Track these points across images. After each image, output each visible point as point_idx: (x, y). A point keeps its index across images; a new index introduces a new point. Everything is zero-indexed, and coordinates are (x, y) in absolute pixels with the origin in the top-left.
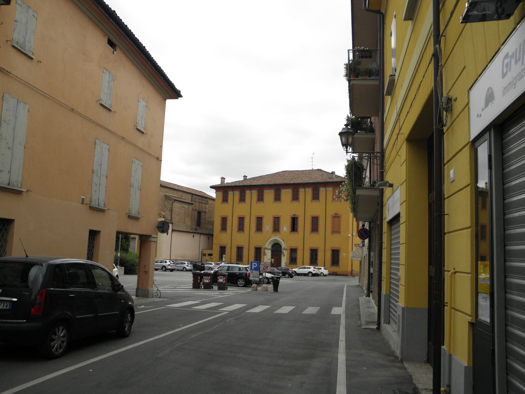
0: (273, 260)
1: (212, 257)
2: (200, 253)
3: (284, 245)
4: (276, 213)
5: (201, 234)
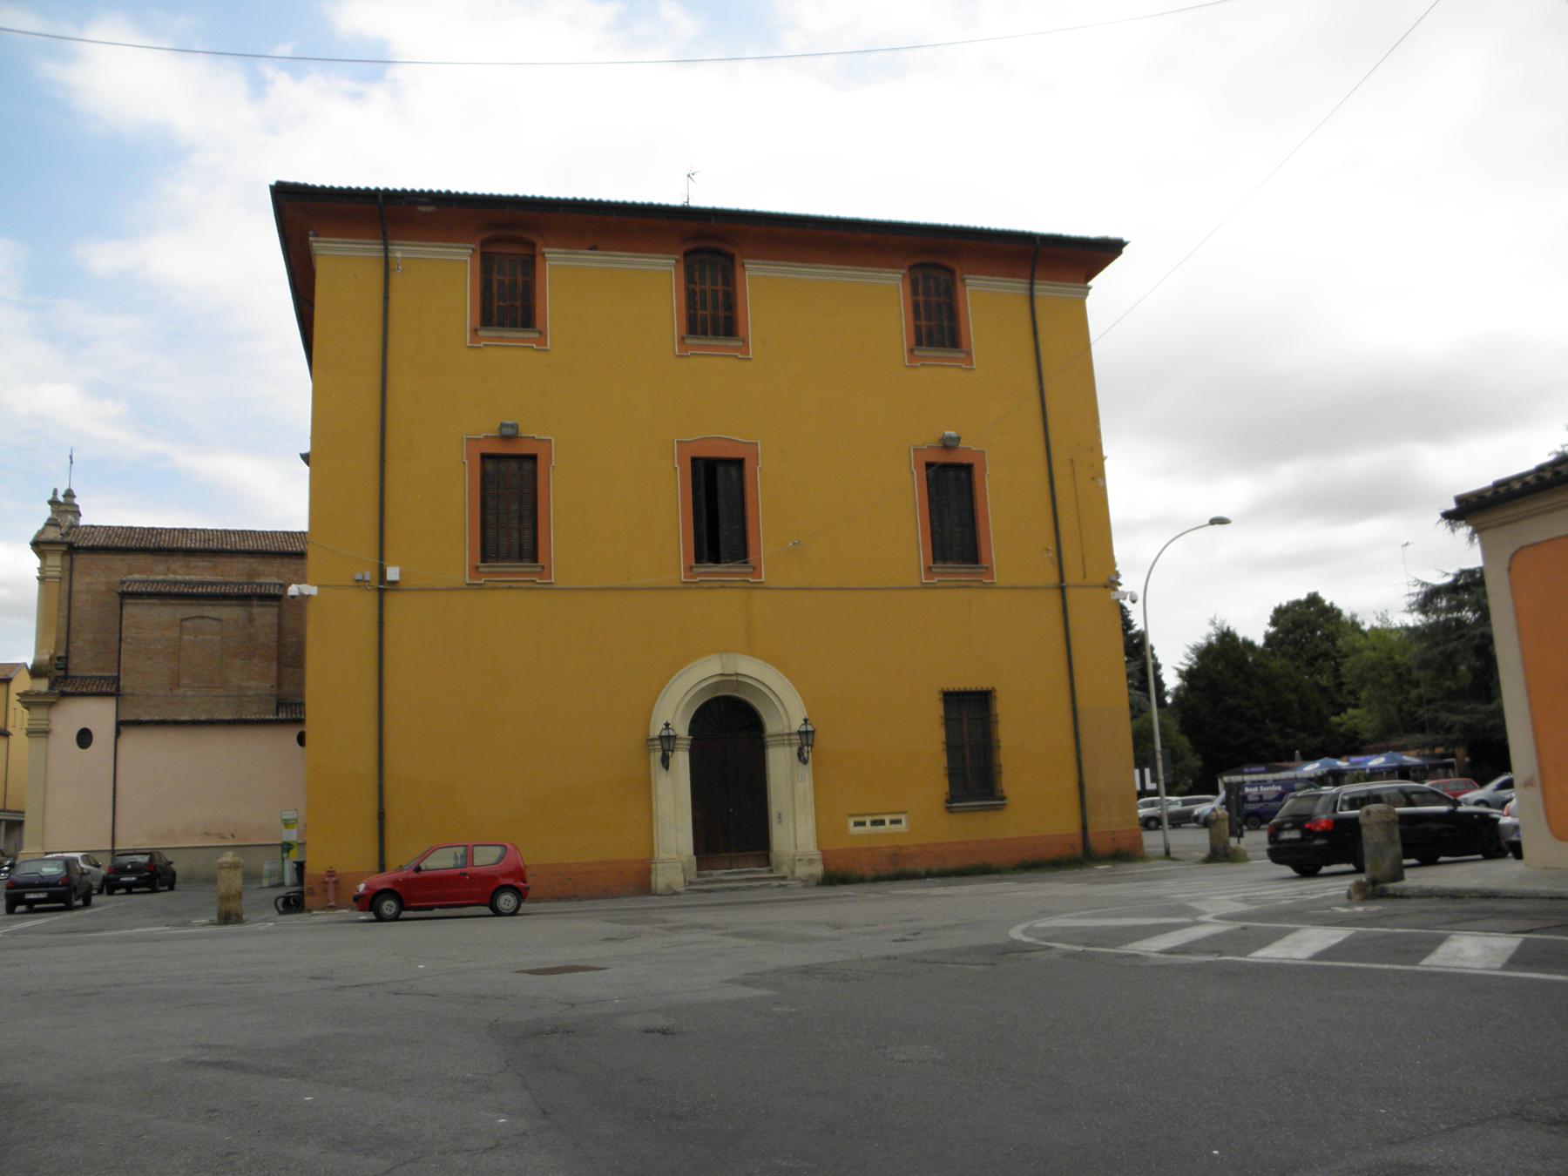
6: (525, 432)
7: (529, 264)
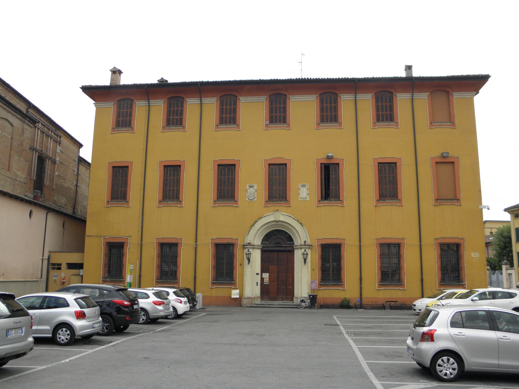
0: (266, 276)
1: (81, 272)
2: (45, 262)
3: (301, 236)
4: (277, 154)
5: (49, 210)
6: (451, 154)
7: (391, 100)
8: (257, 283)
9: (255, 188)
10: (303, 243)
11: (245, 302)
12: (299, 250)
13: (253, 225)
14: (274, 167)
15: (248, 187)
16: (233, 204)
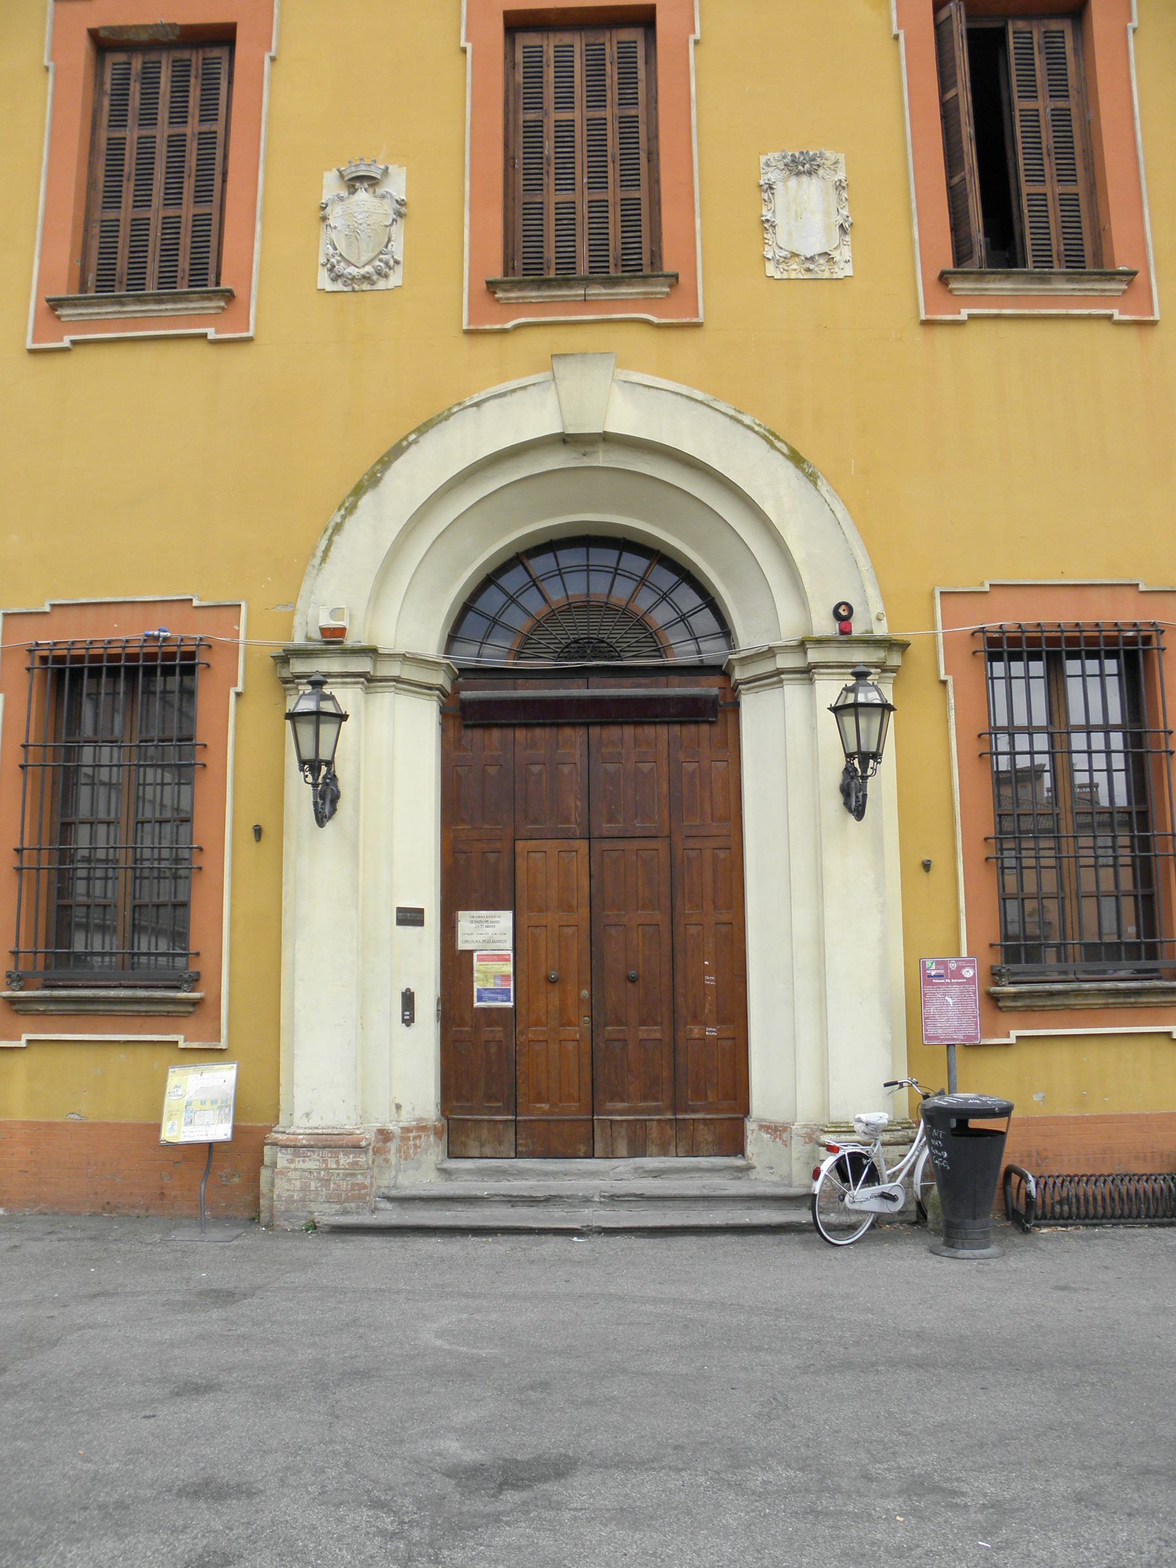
3: (800, 559)
8: (408, 1000)
9: (397, 186)
10: (826, 626)
11: (288, 1179)
12: (793, 691)
13: (371, 480)
14: (549, 44)
15: (331, 185)
16: (204, 319)
